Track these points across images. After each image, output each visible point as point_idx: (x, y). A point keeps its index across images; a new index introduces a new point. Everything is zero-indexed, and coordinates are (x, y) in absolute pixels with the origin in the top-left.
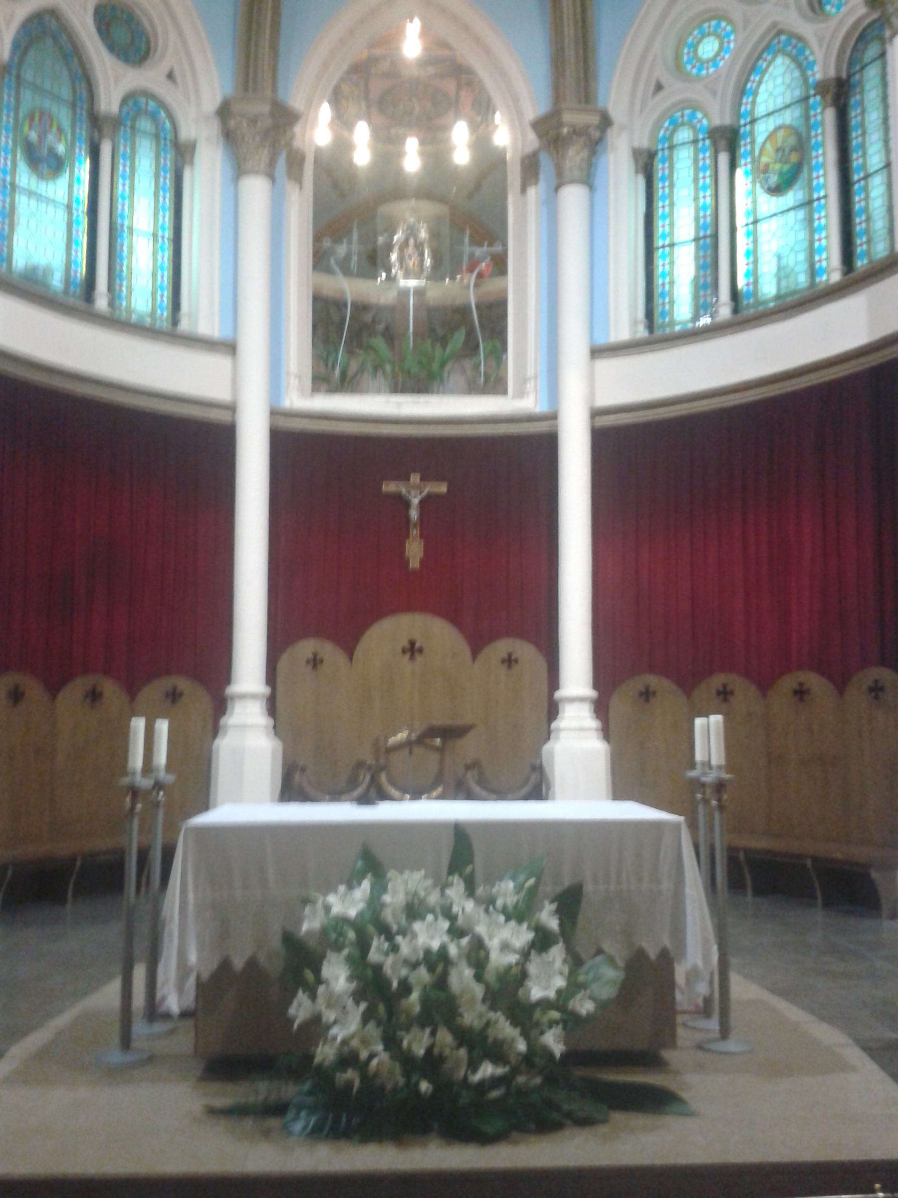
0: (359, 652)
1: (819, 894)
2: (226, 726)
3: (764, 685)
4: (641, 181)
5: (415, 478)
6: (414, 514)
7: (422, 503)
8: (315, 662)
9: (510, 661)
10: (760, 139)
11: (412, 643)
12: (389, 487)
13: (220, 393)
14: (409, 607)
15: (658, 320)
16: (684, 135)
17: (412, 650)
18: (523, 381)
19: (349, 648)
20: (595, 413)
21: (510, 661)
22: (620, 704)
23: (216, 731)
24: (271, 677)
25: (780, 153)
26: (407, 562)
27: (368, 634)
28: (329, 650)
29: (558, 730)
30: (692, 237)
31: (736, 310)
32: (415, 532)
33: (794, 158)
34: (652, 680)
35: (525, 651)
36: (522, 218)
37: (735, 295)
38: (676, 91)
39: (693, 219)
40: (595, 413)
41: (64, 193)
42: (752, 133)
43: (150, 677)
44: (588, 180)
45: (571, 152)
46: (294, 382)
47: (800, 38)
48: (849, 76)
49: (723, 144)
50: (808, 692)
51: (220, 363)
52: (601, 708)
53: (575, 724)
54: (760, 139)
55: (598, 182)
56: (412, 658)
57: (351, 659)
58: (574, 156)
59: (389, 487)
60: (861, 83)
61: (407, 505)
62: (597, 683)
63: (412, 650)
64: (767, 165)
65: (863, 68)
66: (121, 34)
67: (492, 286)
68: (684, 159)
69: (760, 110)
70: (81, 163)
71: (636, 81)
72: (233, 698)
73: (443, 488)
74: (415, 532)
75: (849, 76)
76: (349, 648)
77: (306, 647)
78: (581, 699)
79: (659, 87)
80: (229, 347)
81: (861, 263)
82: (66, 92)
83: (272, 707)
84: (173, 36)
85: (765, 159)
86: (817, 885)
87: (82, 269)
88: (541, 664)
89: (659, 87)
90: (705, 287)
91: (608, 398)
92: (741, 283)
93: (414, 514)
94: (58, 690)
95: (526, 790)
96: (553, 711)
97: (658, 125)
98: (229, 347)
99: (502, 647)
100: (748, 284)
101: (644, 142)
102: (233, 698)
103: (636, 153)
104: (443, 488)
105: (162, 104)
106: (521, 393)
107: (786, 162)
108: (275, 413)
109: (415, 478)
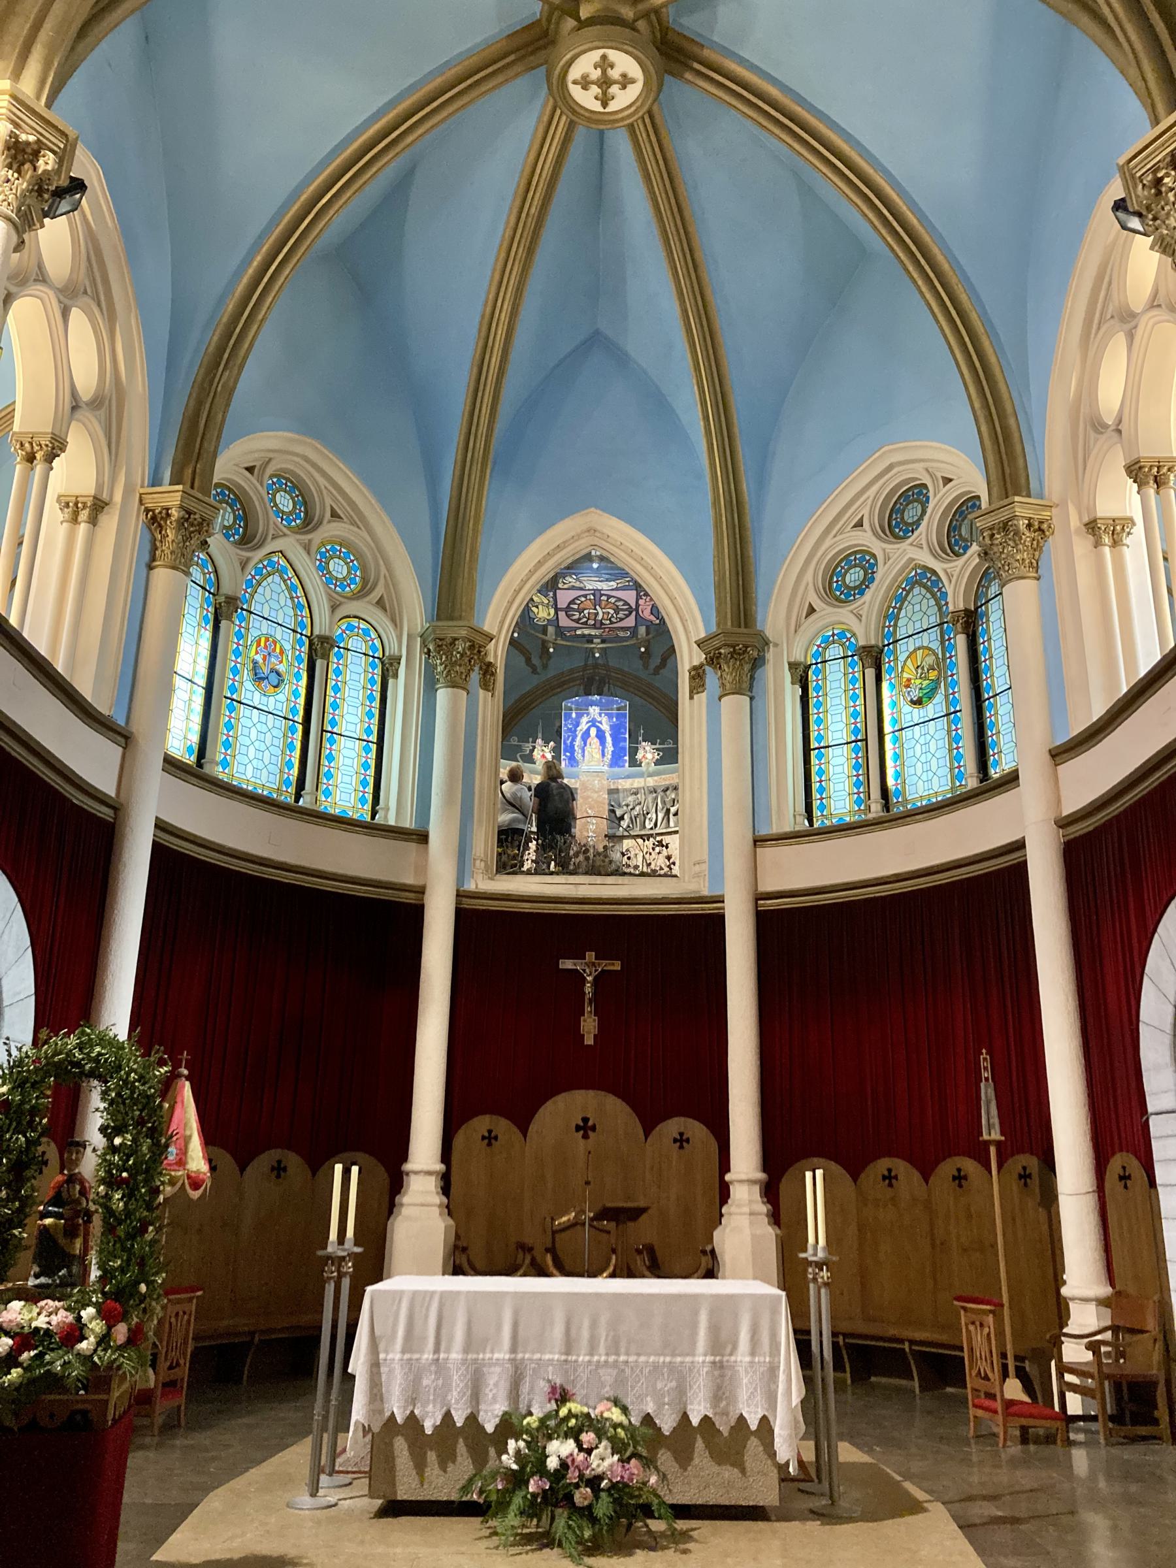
0: (533, 1128)
1: (915, 1374)
2: (402, 1205)
5: (590, 956)
6: (588, 988)
7: (595, 979)
8: (490, 1138)
9: (681, 1141)
10: (902, 658)
11: (585, 1120)
12: (567, 964)
15: (816, 813)
17: (585, 1128)
19: (524, 1128)
21: (681, 1141)
24: (446, 1155)
25: (920, 671)
27: (541, 1110)
28: (503, 1127)
29: (402, 1205)
31: (887, 807)
33: (933, 675)
35: (697, 1130)
37: (885, 792)
39: (628, 1558)
41: (802, 1491)
42: (894, 652)
47: (934, 572)
48: (976, 609)
50: (965, 1178)
54: (902, 658)
57: (525, 1136)
59: (567, 964)
60: (986, 614)
63: (585, 1128)
64: (909, 680)
65: (987, 602)
73: (617, 966)
75: (976, 609)
77: (481, 1124)
78: (429, 1173)
79: (812, 610)
81: (995, 773)
83: (446, 1185)
86: (912, 1362)
89: (812, 610)
90: (923, 575)
92: (890, 782)
93: (588, 988)
94: (318, 1170)
95: (702, 1271)
96: (724, 1193)
98: (421, 837)
99: (673, 1126)
100: (897, 784)
102: (407, 1174)
104: (617, 966)
107: (926, 678)
108: (460, 895)
109: (590, 956)
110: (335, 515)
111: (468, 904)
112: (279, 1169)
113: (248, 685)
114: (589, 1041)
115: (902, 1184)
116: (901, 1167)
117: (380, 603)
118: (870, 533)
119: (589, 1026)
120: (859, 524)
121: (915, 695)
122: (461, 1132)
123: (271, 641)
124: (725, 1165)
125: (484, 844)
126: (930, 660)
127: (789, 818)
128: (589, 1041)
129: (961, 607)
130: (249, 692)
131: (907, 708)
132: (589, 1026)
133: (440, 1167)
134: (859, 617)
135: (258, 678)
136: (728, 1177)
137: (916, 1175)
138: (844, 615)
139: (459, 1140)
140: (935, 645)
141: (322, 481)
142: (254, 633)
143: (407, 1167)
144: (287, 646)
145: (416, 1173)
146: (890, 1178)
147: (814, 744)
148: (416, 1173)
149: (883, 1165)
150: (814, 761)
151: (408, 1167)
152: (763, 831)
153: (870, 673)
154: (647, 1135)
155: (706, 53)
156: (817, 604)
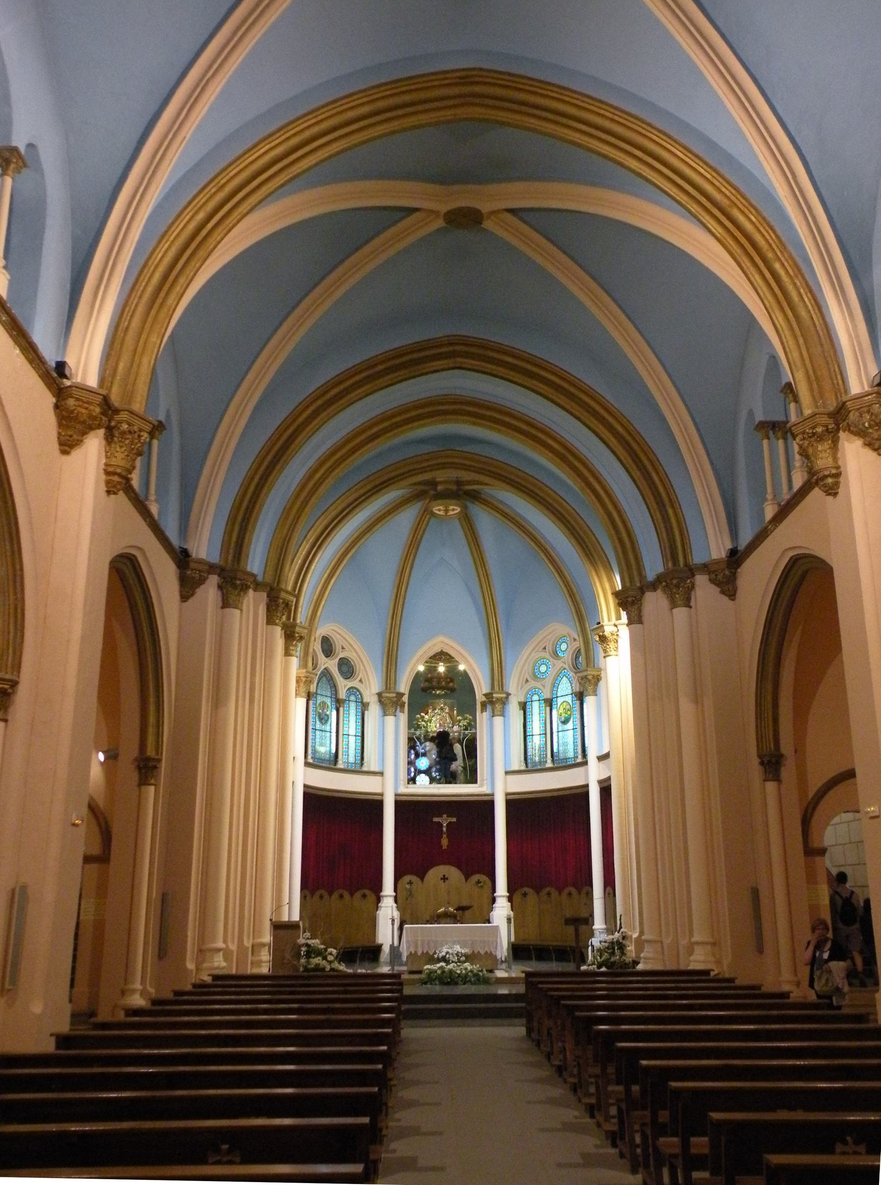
3: (560, 890)
4: (522, 712)
5: (445, 816)
6: (444, 829)
8: (410, 883)
10: (559, 704)
11: (444, 876)
12: (436, 820)
13: (378, 790)
14: (444, 863)
16: (536, 697)
17: (444, 878)
18: (483, 780)
19: (422, 879)
20: (507, 794)
22: (517, 897)
23: (377, 908)
26: (442, 847)
28: (414, 878)
30: (570, 692)
32: (445, 836)
33: (569, 713)
34: (526, 889)
35: (484, 878)
36: (481, 721)
38: (532, 683)
40: (507, 794)
42: (557, 701)
43: (358, 889)
44: (503, 715)
45: (497, 706)
46: (402, 782)
49: (548, 704)
51: (378, 778)
52: (510, 899)
53: (501, 905)
55: (506, 714)
56: (444, 882)
58: (498, 706)
59: (436, 820)
61: (442, 826)
62: (509, 890)
63: (444, 878)
66: (345, 669)
67: (461, 777)
68: (536, 705)
69: (559, 694)
70: (276, 610)
71: (519, 679)
72: (383, 896)
73: (454, 820)
74: (445, 836)
76: (422, 879)
77: (407, 878)
78: (503, 896)
79: (527, 681)
80: (381, 774)
82: (329, 694)
84: (362, 667)
85: (560, 711)
87: (333, 751)
88: (489, 883)
89: (527, 681)
91: (512, 789)
92: (555, 750)
93: (444, 829)
96: (494, 900)
97: (527, 693)
99: (476, 877)
101: (522, 700)
102: (383, 896)
103: (520, 703)
104: (454, 820)
105: (358, 690)
106: (482, 786)
109: (445, 816)
110: (343, 648)
111: (510, 797)
112: (341, 896)
113: (318, 722)
114: (445, 847)
115: (553, 896)
116: (553, 890)
117: (361, 681)
118: (548, 654)
119: (445, 842)
120: (545, 648)
121: (563, 719)
122: (400, 882)
123: (324, 703)
124: (494, 890)
125: (403, 776)
126: (568, 707)
127: (517, 763)
128: (445, 847)
129: (578, 690)
130: (318, 725)
131: (560, 724)
132: (445, 842)
133: (394, 894)
134: (544, 686)
135: (321, 719)
136: (495, 895)
137: (557, 893)
138: (538, 685)
139: (399, 885)
140: (570, 702)
141: (338, 636)
142: (319, 702)
143: (382, 894)
144: (329, 704)
145: (387, 896)
146: (549, 894)
147: (528, 734)
148: (387, 896)
149: (548, 889)
150: (528, 740)
151: (382, 894)
152: (508, 770)
153: (548, 709)
154: (466, 881)
155: (483, 496)
156: (529, 679)
